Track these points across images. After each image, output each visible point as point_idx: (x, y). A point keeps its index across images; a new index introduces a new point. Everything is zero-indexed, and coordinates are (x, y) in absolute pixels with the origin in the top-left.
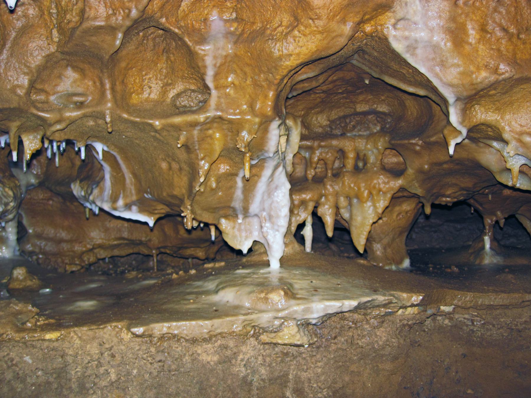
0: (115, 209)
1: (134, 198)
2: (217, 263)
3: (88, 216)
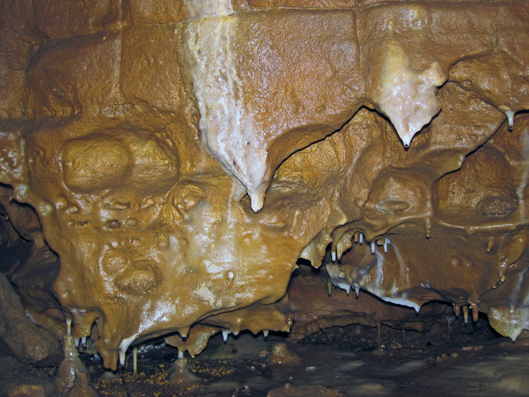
0: (388, 296)
1: (409, 286)
2: (475, 347)
3: (330, 293)
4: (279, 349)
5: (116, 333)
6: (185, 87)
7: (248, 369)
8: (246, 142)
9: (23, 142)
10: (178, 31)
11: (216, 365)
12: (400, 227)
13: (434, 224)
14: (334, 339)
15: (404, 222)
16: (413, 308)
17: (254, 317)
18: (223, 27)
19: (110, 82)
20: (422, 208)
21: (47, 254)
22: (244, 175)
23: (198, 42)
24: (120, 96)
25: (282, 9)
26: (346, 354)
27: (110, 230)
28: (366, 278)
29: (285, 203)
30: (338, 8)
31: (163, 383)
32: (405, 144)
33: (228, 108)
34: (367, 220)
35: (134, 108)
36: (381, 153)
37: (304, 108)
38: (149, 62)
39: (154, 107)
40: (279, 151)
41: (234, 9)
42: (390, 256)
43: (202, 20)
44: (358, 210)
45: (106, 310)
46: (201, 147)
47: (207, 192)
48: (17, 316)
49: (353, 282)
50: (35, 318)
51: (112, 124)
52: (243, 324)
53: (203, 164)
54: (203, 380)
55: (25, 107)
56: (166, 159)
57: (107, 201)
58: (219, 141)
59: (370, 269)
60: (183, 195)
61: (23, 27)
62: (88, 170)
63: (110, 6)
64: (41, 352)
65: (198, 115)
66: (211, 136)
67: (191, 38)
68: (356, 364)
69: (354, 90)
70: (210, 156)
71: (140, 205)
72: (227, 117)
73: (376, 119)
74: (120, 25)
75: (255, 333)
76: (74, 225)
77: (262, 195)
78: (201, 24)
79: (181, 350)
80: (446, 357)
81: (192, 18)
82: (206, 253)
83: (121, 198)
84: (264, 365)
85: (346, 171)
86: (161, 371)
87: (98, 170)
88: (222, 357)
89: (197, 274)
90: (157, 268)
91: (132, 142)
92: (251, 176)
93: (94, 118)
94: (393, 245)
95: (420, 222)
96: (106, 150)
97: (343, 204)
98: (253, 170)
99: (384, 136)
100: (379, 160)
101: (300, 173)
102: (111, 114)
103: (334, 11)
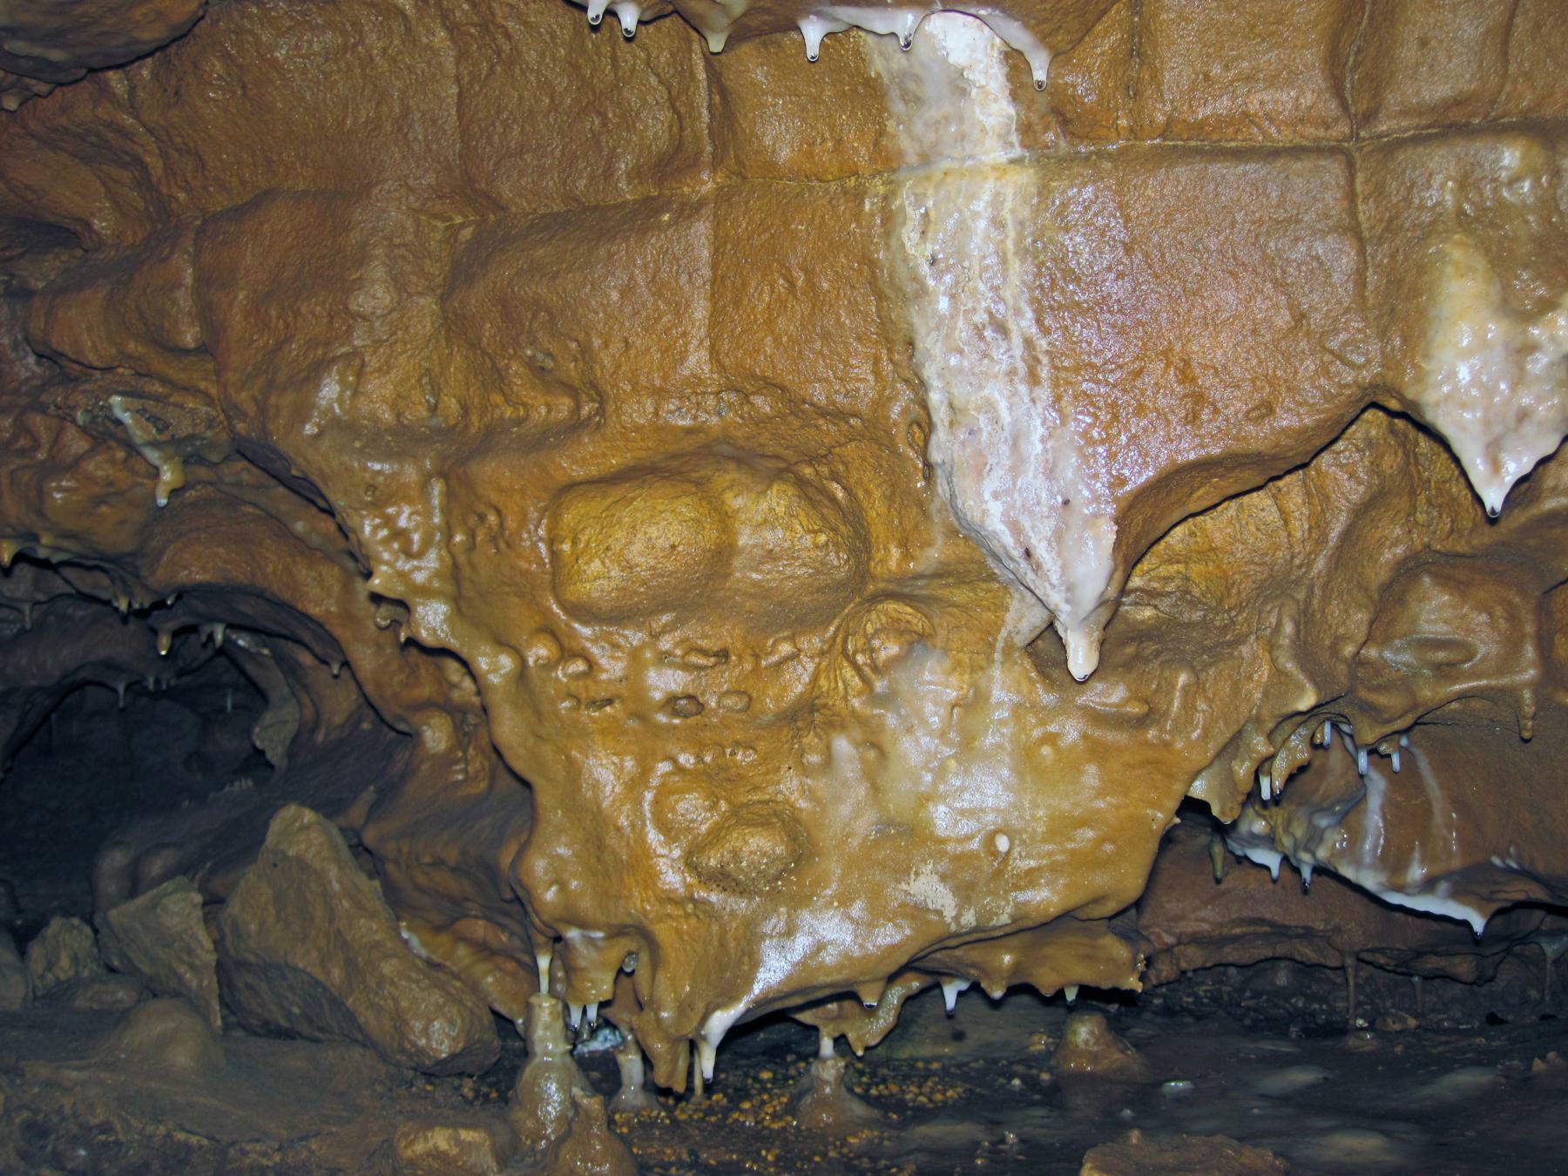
0: (1399, 889)
1: (1456, 863)
4: (1084, 1032)
5: (690, 994)
6: (890, 351)
7: (1002, 1086)
8: (1060, 499)
9: (437, 488)
10: (873, 204)
11: (910, 1073)
12: (1446, 709)
13: (1543, 703)
14: (1216, 1000)
15: (1462, 696)
16: (1465, 924)
17: (1048, 951)
18: (997, 194)
19: (684, 334)
20: (1509, 660)
21: (458, 772)
22: (1053, 586)
23: (930, 235)
24: (711, 371)
25: (1153, 147)
26: (1268, 1046)
27: (677, 721)
28: (1335, 840)
29: (1147, 652)
30: (1305, 143)
31: (781, 1124)
32: (1488, 508)
33: (1010, 409)
34: (1363, 694)
35: (748, 402)
36: (1402, 514)
37: (1216, 411)
38: (792, 284)
39: (804, 402)
40: (1145, 521)
41: (1023, 145)
42: (1405, 782)
43: (938, 176)
44: (1342, 668)
45: (662, 932)
46: (933, 508)
47: (936, 621)
48: (378, 937)
49: (1296, 848)
50: (425, 944)
51: (688, 444)
52: (1017, 967)
53: (935, 554)
54: (886, 1116)
55: (436, 391)
56: (821, 531)
57: (666, 644)
58: (987, 496)
59: (1345, 814)
60: (870, 629)
61: (430, 179)
62: (612, 561)
63: (675, 129)
64: (448, 1035)
65: (926, 425)
66: (964, 483)
67: (910, 225)
68: (1302, 1077)
69: (1353, 366)
70: (958, 532)
71: (757, 657)
72: (1007, 433)
73: (1391, 425)
74: (707, 183)
75: (1047, 992)
76: (577, 708)
77: (1096, 635)
78: (937, 188)
79: (828, 1035)
80: (1559, 1061)
81: (912, 168)
82: (935, 784)
83: (704, 636)
84: (1045, 1076)
85: (1309, 564)
86: (764, 1090)
87: (640, 560)
88: (926, 1050)
89: (906, 837)
90: (797, 821)
91: (731, 487)
92: (1070, 588)
93: (638, 429)
94: (1413, 750)
95: (1507, 696)
96: (660, 507)
97: (1304, 652)
98: (1074, 571)
99: (1412, 468)
100: (1398, 531)
101: (1181, 567)
102: (684, 418)
103: (1296, 152)
